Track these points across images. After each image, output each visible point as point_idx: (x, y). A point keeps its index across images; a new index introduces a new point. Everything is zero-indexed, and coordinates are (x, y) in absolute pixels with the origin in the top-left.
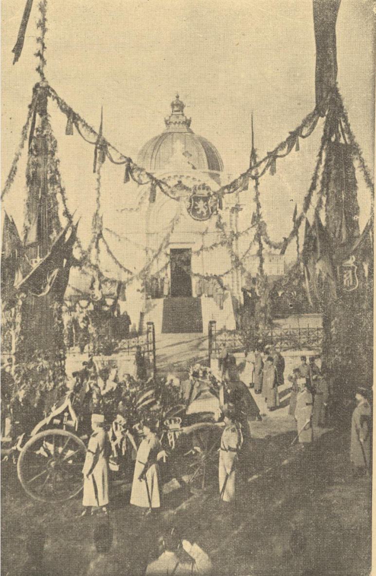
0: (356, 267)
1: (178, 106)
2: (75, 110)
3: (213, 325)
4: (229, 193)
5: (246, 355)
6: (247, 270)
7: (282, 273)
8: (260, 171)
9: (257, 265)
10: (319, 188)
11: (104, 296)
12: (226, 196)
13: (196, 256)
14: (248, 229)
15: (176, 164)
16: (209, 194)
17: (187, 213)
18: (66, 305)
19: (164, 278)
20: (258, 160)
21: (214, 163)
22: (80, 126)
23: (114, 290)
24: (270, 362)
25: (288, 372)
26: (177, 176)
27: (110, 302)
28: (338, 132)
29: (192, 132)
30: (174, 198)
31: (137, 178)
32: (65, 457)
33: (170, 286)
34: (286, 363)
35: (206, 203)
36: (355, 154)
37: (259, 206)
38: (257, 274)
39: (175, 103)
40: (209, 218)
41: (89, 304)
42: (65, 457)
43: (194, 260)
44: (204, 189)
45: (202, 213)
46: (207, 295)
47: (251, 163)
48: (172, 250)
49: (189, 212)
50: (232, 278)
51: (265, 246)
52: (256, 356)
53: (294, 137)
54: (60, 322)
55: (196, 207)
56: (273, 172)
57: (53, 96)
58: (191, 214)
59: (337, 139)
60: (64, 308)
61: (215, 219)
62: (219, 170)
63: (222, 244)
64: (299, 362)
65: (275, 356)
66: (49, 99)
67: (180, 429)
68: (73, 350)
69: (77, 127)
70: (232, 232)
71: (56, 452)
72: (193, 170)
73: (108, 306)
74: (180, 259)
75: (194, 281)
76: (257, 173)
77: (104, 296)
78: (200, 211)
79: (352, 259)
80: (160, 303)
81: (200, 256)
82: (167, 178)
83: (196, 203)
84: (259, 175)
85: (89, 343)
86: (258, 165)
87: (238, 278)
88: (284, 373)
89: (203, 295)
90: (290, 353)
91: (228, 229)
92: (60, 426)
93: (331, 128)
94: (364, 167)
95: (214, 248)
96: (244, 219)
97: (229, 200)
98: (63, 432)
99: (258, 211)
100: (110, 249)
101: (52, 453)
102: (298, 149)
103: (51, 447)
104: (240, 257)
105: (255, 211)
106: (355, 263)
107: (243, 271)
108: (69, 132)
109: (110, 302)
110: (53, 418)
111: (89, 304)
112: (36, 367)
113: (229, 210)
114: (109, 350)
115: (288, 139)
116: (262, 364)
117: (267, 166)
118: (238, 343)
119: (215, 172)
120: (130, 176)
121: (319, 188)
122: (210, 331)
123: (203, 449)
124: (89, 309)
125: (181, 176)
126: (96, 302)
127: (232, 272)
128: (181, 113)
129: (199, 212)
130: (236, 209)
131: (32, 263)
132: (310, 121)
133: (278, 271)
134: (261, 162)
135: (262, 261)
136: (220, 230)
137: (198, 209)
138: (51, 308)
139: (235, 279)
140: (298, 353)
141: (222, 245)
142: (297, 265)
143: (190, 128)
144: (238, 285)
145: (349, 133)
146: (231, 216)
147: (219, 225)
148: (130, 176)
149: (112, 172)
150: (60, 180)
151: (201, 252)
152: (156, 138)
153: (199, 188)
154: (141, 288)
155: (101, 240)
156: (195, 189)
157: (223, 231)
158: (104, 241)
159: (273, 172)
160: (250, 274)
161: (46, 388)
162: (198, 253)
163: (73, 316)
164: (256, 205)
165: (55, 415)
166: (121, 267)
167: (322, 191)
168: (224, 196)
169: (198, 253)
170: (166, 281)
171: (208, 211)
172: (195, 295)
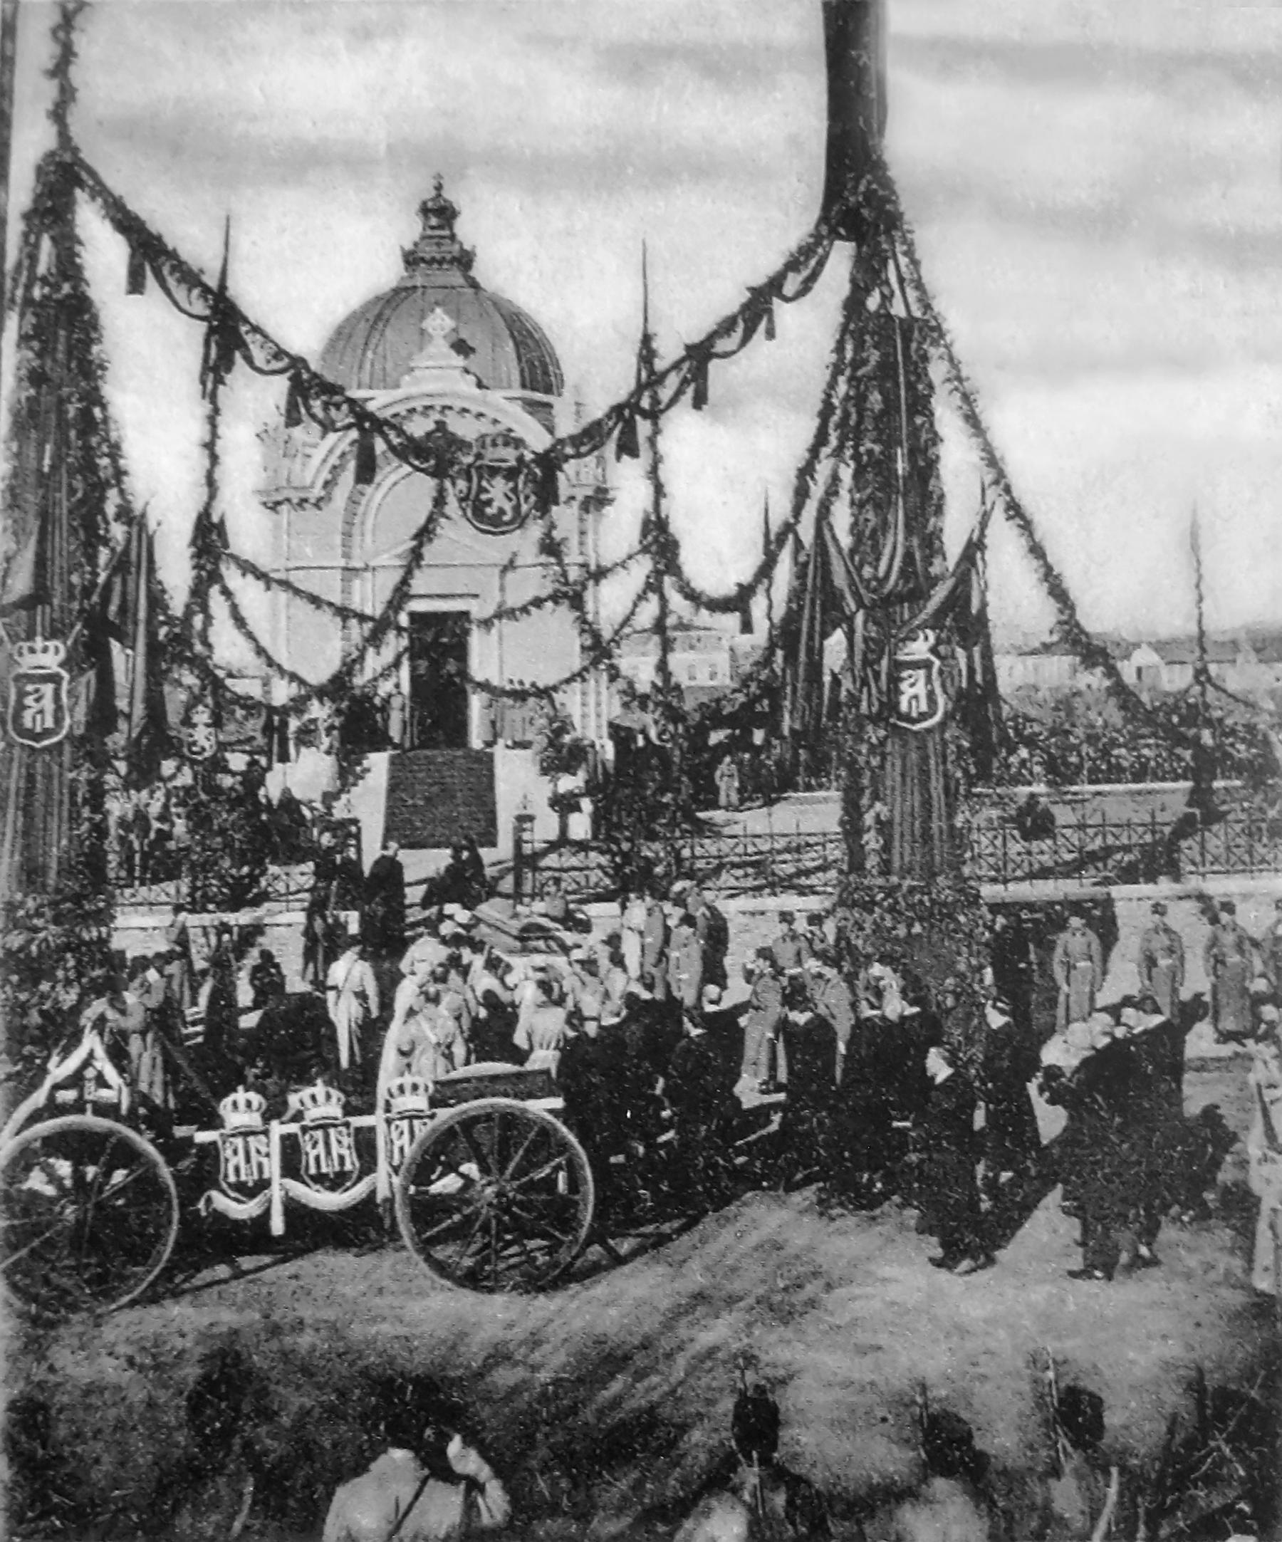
0: (937, 663)
2: (155, 226)
3: (527, 825)
5: (624, 907)
7: (725, 680)
9: (654, 659)
10: (833, 441)
11: (223, 746)
14: (630, 557)
15: (431, 380)
16: (520, 459)
18: (117, 773)
19: (390, 696)
20: (660, 365)
21: (540, 373)
22: (166, 270)
23: (254, 726)
24: (686, 930)
26: (431, 407)
27: (238, 761)
28: (887, 283)
30: (422, 470)
31: (319, 412)
33: (407, 715)
35: (511, 485)
36: (935, 343)
37: (659, 490)
38: (654, 685)
39: (430, 205)
40: (520, 527)
41: (179, 769)
43: (476, 640)
44: (506, 444)
45: (502, 512)
46: (510, 743)
49: (464, 510)
50: (584, 694)
51: (677, 601)
52: (650, 912)
54: (98, 817)
55: (484, 497)
56: (699, 401)
57: (92, 188)
59: (886, 299)
60: (111, 779)
62: (548, 390)
63: (555, 598)
64: (771, 932)
65: (700, 912)
68: (133, 895)
70: (584, 566)
71: (78, 1176)
72: (477, 391)
73: (234, 774)
75: (476, 702)
76: (655, 400)
78: (495, 504)
79: (926, 638)
80: (378, 763)
81: (494, 631)
83: (484, 483)
84: (662, 407)
85: (179, 877)
88: (727, 961)
89: (501, 742)
91: (572, 557)
93: (868, 272)
94: (959, 379)
95: (533, 609)
96: (619, 530)
97: (576, 475)
98: (89, 1120)
102: (770, 334)
103: (64, 1168)
104: (607, 634)
105: (650, 509)
106: (934, 650)
107: (614, 674)
108: (136, 285)
109: (238, 761)
110: (57, 1087)
112: (30, 942)
113: (575, 504)
114: (241, 895)
115: (746, 307)
116: (667, 930)
117: (685, 382)
118: (596, 875)
119: (539, 396)
120: (303, 410)
121: (833, 441)
122: (518, 843)
123: (485, 1170)
124: (178, 782)
127: (584, 680)
128: (446, 233)
130: (599, 499)
131: (21, 654)
132: (805, 262)
133: (713, 676)
134: (667, 372)
135: (667, 646)
136: (552, 560)
137: (489, 503)
139: (591, 700)
140: (772, 903)
141: (556, 603)
142: (767, 661)
144: (598, 716)
145: (919, 286)
146: (581, 520)
147: (551, 547)
148: (303, 410)
150: (106, 420)
151: (496, 621)
153: (494, 444)
154: (1077, 1263)
155: (215, 591)
156: (483, 447)
157: (560, 563)
158: (226, 593)
160: (631, 684)
161: (56, 1001)
162: (487, 624)
164: (651, 489)
165: (58, 1080)
168: (565, 466)
169: (487, 624)
170: (396, 702)
171: (517, 508)
172: (476, 742)
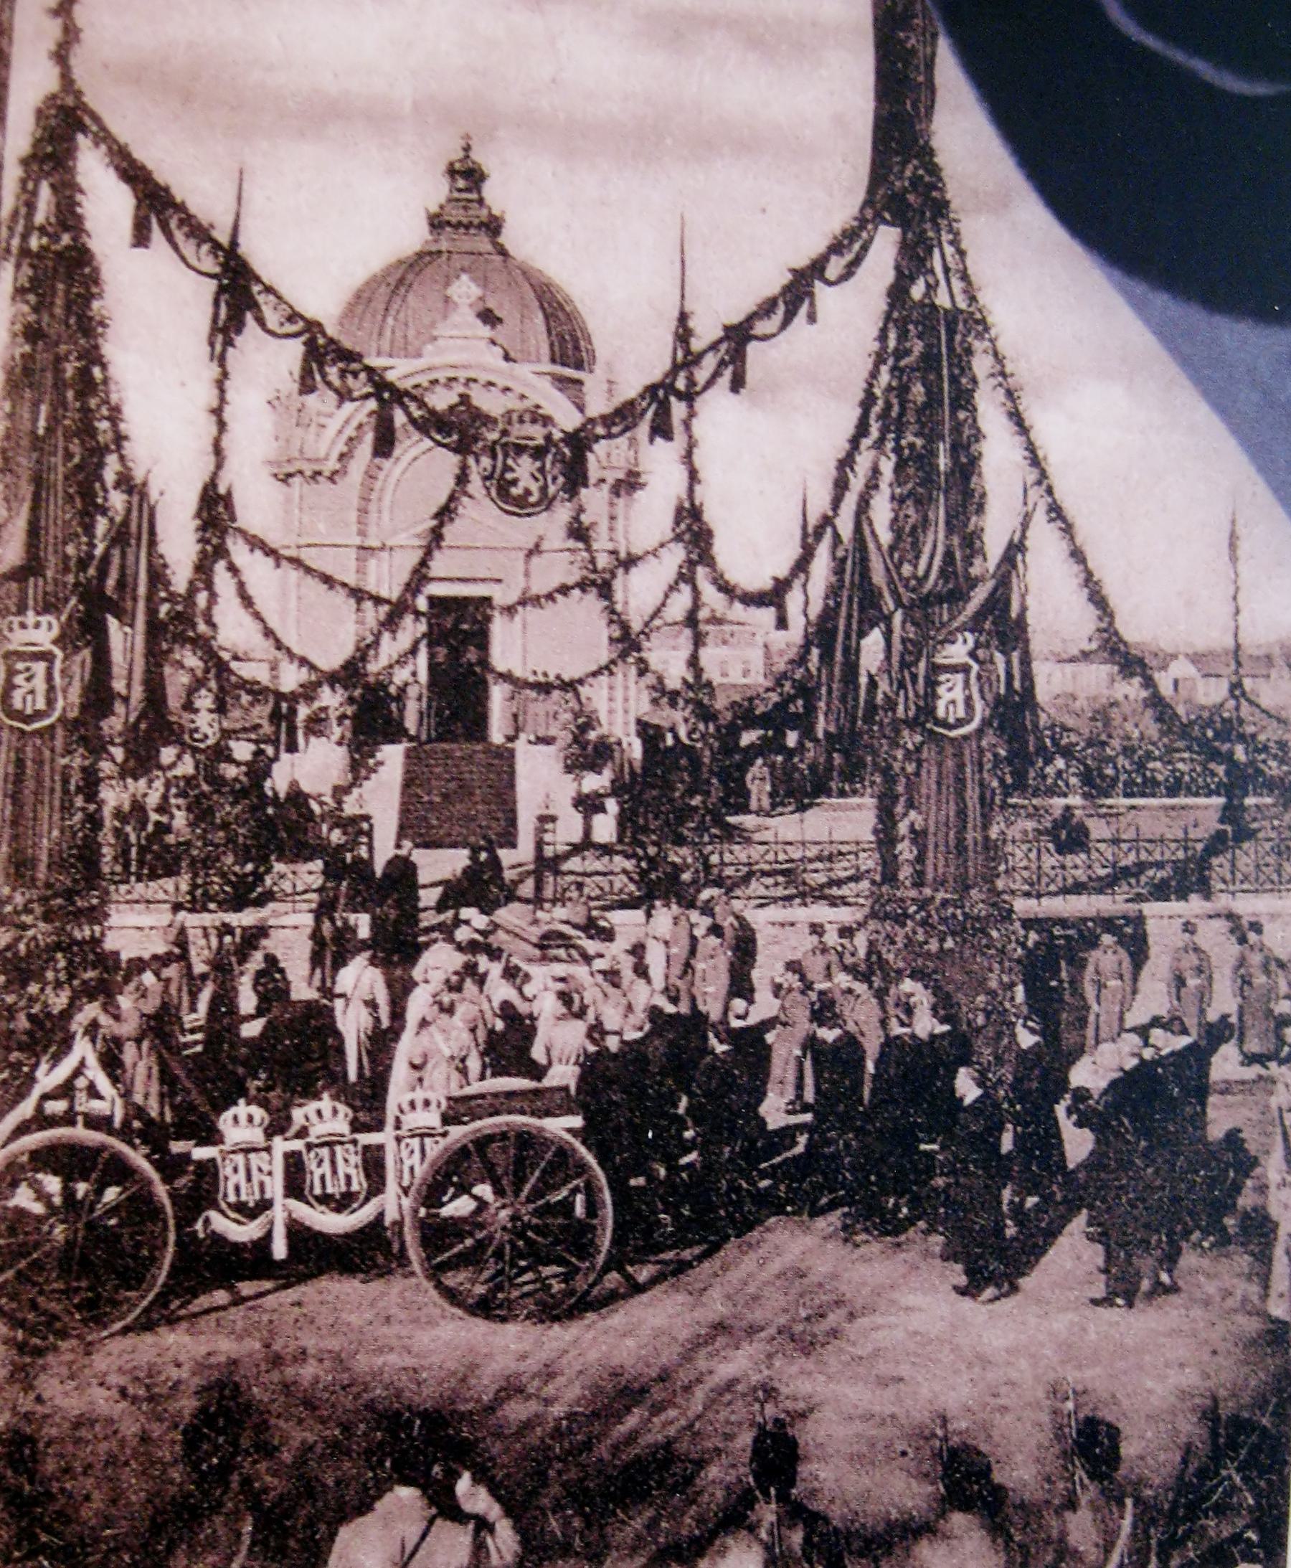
1: (468, 176)
3: (549, 826)
4: (609, 436)
6: (653, 666)
7: (758, 679)
8: (702, 375)
10: (875, 432)
11: (226, 734)
12: (600, 448)
13: (506, 618)
14: (662, 545)
15: (449, 349)
16: (548, 438)
17: (484, 492)
18: (113, 761)
19: (406, 684)
21: (570, 349)
23: (260, 714)
24: (713, 941)
25: (765, 971)
27: (242, 750)
29: (503, 252)
30: (444, 446)
31: (337, 382)
32: (99, 1210)
33: (424, 705)
34: (760, 942)
35: (538, 464)
36: (979, 336)
37: (693, 476)
38: (685, 681)
39: (457, 166)
40: (547, 509)
41: (179, 757)
42: (99, 1210)
43: (499, 629)
44: (534, 421)
46: (532, 738)
47: (675, 353)
48: (432, 600)
50: (611, 688)
51: (710, 594)
52: (676, 920)
53: (797, 293)
54: (92, 807)
55: (509, 476)
56: (737, 384)
57: (95, 135)
58: (494, 493)
59: (931, 288)
60: (106, 767)
61: (563, 513)
62: (579, 366)
63: (583, 585)
65: (728, 922)
66: (83, 141)
67: (349, 1137)
68: (129, 892)
69: (165, 227)
71: (68, 1193)
72: (504, 364)
73: (238, 764)
74: (459, 630)
75: (498, 694)
76: (691, 382)
77: (226, 734)
78: (521, 484)
80: (392, 756)
82: (425, 384)
84: (698, 388)
86: (697, 359)
87: (626, 700)
88: (755, 974)
89: (523, 736)
90: (775, 913)
91: (601, 542)
92: (68, 1119)
93: (914, 258)
94: (1003, 374)
95: (559, 597)
96: (649, 519)
97: (606, 458)
98: (80, 1133)
99: (691, 491)
100: (251, 591)
101: (57, 1200)
102: (812, 318)
103: (53, 1184)
104: (636, 626)
105: (684, 496)
106: (972, 654)
108: (141, 238)
109: (242, 750)
110: (45, 1097)
111: (179, 757)
113: (606, 488)
115: (787, 289)
116: (694, 939)
117: (722, 364)
119: (569, 372)
120: (318, 377)
121: (875, 432)
122: (540, 845)
123: (499, 1192)
124: (178, 772)
125: (470, 380)
126: (203, 751)
127: (611, 673)
128: (474, 196)
129: (515, 491)
130: (630, 483)
132: (850, 244)
133: (746, 673)
134: (705, 352)
136: (581, 545)
138: (66, 767)
139: (619, 694)
141: (584, 591)
142: (802, 660)
143: (501, 240)
145: (965, 277)
146: (612, 504)
148: (318, 377)
149: (267, 360)
150: (106, 381)
151: (520, 608)
152: (400, 262)
153: (521, 421)
156: (510, 423)
157: (588, 549)
158: (233, 569)
159: (737, 384)
160: (660, 679)
161: (46, 1005)
162: (510, 610)
163: (132, 790)
164: (685, 475)
165: (48, 1089)
166: (279, 645)
167: (880, 442)
169: (510, 610)
170: (413, 691)
171: (544, 489)
172: (497, 735)
